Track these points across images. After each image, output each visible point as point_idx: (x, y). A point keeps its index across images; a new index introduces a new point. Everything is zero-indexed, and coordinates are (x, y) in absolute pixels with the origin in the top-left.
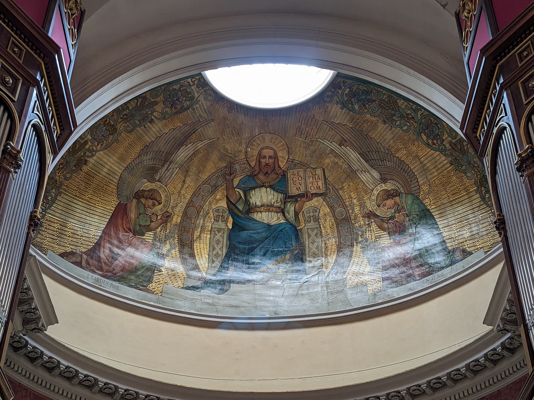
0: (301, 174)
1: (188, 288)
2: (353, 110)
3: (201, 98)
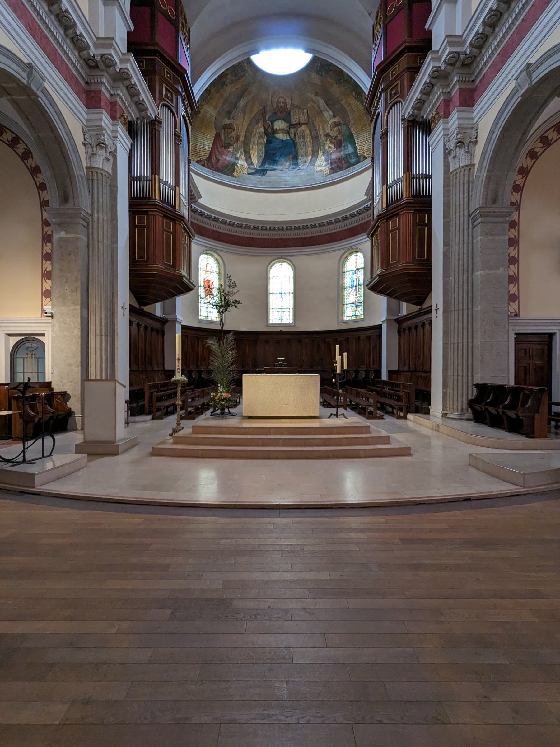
0: (297, 112)
1: (249, 174)
2: (321, 75)
3: (249, 70)
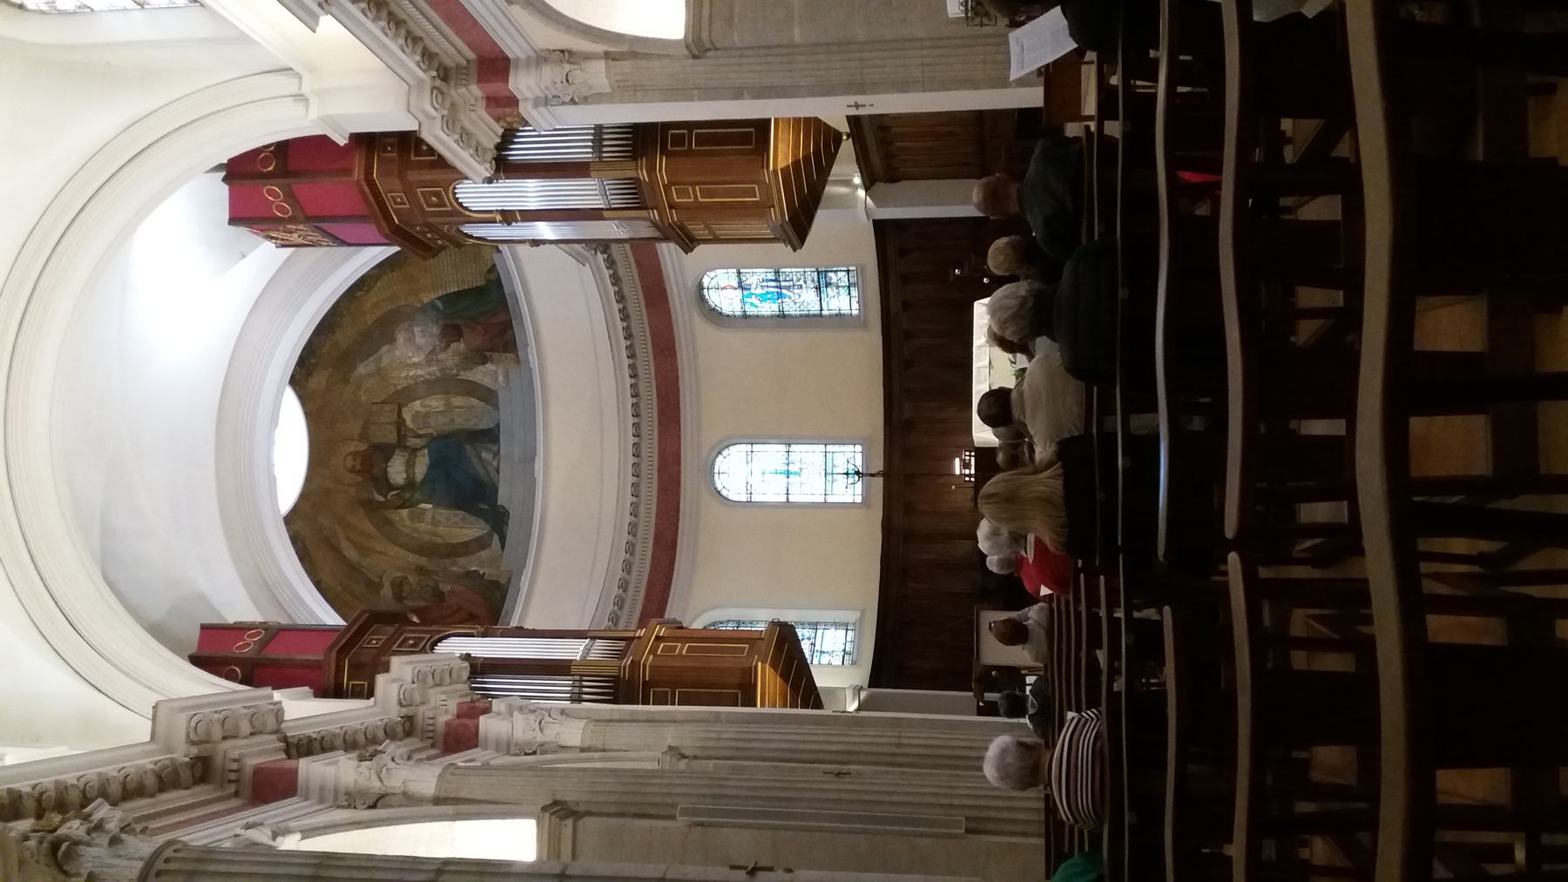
1: (503, 547)
